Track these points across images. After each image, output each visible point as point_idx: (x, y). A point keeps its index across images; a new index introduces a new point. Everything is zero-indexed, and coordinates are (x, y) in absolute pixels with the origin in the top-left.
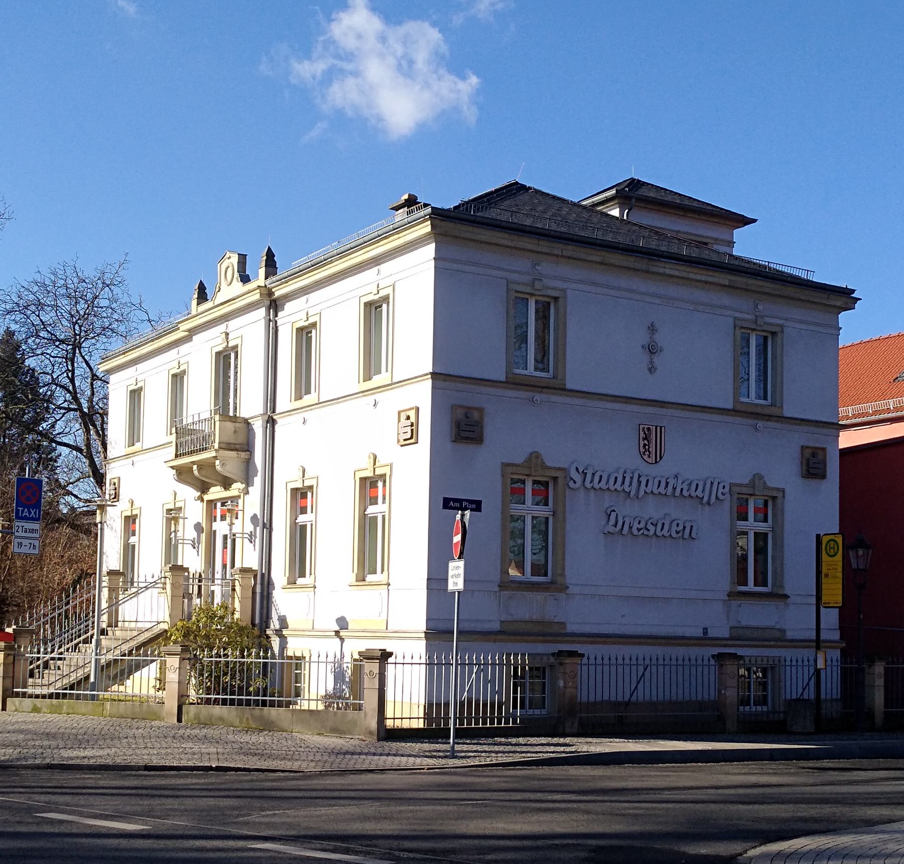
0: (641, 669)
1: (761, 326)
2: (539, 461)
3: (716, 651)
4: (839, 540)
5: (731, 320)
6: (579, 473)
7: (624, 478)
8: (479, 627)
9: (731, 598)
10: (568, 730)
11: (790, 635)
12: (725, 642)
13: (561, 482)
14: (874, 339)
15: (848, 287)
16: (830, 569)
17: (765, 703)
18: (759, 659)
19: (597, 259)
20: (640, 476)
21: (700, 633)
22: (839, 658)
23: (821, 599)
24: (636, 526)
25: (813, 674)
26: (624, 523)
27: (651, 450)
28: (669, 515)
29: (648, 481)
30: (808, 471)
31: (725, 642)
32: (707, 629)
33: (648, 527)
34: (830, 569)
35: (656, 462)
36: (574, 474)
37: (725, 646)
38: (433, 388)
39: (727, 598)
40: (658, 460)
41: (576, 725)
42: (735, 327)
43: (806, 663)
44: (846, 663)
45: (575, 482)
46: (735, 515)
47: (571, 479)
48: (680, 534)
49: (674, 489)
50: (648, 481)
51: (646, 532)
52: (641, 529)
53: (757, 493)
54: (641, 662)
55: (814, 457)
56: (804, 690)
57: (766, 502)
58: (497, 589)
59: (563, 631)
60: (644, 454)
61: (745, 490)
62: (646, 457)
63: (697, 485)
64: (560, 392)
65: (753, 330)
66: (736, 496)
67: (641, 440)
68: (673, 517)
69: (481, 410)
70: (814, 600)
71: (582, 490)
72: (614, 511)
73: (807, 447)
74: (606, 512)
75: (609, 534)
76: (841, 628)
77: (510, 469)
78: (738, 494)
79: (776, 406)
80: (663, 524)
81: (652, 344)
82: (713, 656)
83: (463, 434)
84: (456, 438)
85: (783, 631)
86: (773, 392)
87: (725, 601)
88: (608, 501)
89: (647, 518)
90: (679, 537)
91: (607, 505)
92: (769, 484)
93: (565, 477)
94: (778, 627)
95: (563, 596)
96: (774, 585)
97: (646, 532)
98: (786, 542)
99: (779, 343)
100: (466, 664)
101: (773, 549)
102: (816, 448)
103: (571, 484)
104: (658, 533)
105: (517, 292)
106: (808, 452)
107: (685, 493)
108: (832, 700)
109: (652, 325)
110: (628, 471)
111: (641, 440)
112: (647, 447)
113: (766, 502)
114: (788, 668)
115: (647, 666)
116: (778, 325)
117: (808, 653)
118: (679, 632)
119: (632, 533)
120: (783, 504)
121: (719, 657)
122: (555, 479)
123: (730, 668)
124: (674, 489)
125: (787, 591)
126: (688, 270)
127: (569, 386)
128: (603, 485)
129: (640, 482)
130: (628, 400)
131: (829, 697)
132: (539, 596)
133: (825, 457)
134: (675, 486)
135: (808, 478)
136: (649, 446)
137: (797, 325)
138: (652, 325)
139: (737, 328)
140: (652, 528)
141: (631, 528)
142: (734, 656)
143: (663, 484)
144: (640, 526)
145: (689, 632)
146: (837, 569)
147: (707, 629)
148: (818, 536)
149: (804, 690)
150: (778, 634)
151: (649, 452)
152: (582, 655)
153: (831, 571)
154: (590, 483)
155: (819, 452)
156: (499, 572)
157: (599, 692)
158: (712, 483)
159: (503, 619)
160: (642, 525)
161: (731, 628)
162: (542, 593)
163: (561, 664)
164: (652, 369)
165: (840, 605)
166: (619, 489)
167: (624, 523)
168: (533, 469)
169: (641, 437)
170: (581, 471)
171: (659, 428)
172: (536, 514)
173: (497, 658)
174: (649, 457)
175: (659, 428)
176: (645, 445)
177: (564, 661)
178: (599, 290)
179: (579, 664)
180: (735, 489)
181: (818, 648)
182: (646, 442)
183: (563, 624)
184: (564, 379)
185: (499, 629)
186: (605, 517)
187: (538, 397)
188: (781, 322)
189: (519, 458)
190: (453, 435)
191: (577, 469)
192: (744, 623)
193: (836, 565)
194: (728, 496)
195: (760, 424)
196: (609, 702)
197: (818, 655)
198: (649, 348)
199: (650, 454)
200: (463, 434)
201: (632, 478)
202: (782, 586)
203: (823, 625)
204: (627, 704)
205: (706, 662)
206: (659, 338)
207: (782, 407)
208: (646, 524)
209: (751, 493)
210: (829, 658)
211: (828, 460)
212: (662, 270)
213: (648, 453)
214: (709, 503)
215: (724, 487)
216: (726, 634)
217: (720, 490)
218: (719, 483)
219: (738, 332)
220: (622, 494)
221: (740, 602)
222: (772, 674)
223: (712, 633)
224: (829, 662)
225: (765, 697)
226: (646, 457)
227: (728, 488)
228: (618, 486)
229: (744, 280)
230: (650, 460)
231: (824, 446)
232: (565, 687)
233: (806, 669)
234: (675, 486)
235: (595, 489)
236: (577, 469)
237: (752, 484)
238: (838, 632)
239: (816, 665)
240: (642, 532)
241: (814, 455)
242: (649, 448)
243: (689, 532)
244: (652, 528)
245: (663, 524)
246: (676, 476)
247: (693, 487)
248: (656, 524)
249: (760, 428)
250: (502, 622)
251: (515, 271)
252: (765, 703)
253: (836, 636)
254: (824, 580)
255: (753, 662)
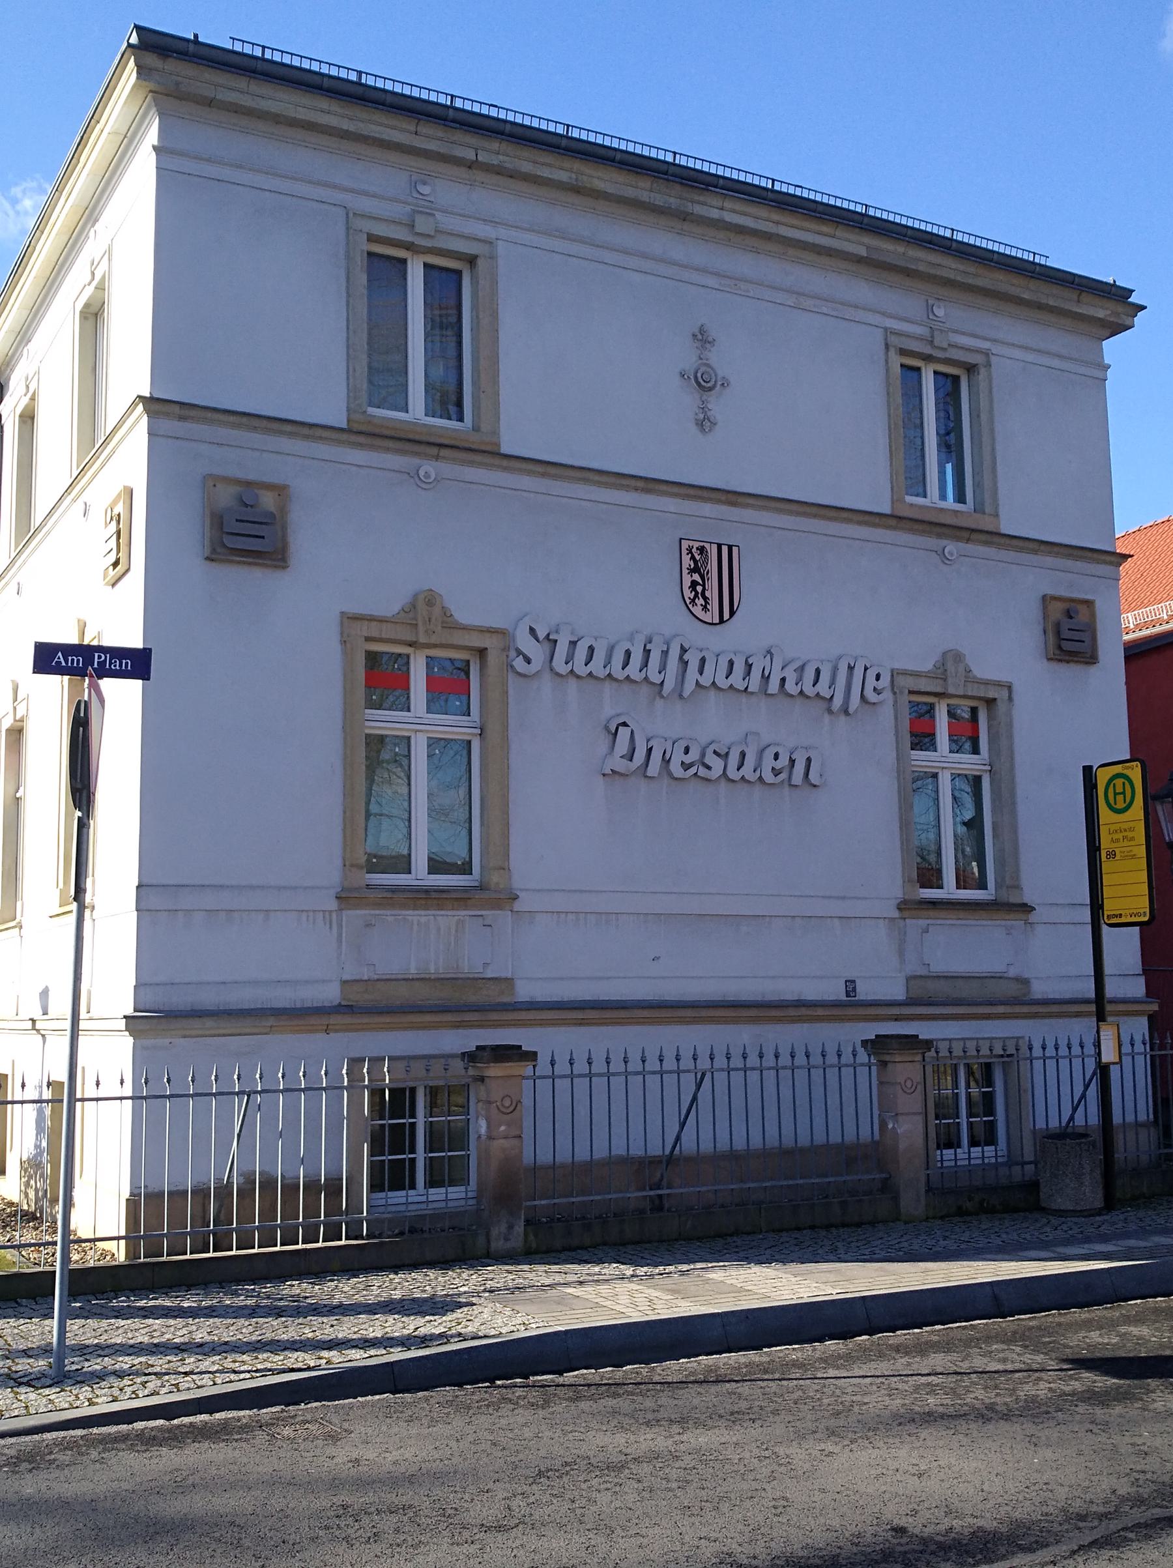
0: (688, 1081)
1: (944, 349)
2: (437, 611)
3: (872, 1030)
4: (1135, 772)
5: (879, 335)
6: (538, 641)
7: (647, 652)
8: (283, 998)
9: (906, 914)
10: (497, 1245)
11: (1039, 990)
12: (895, 1011)
13: (493, 658)
14: (1159, 521)
15: (1117, 283)
16: (1118, 840)
17: (991, 1140)
18: (971, 1046)
19: (563, 176)
20: (684, 650)
21: (835, 991)
22: (1147, 1038)
23: (1102, 907)
24: (678, 758)
25: (1094, 1073)
26: (650, 750)
27: (708, 594)
28: (757, 734)
29: (703, 661)
30: (1060, 648)
31: (895, 1011)
32: (853, 982)
33: (707, 761)
34: (1118, 840)
35: (722, 621)
36: (526, 643)
37: (897, 1019)
38: (151, 433)
39: (896, 914)
40: (726, 616)
41: (520, 1228)
42: (887, 346)
43: (1076, 1050)
44: (1162, 1047)
45: (528, 661)
46: (907, 740)
47: (519, 653)
48: (783, 776)
49: (766, 678)
50: (703, 661)
51: (702, 772)
52: (691, 765)
53: (951, 690)
54: (688, 1063)
55: (1071, 617)
56: (1075, 1109)
57: (974, 711)
58: (333, 905)
59: (506, 999)
60: (693, 601)
61: (924, 685)
62: (697, 610)
63: (818, 672)
64: (487, 459)
65: (928, 358)
66: (905, 698)
67: (685, 571)
68: (766, 738)
69: (281, 490)
70: (1086, 915)
71: (547, 676)
72: (625, 724)
73: (1055, 598)
74: (607, 728)
75: (617, 777)
76: (1148, 971)
77: (365, 629)
78: (910, 692)
79: (984, 513)
80: (743, 755)
81: (703, 369)
82: (865, 1043)
83: (230, 542)
84: (214, 551)
85: (1025, 982)
86: (977, 485)
87: (892, 919)
88: (610, 704)
89: (704, 741)
90: (782, 782)
91: (608, 710)
92: (978, 673)
93: (506, 649)
94: (1012, 973)
95: (503, 918)
96: (998, 886)
97: (702, 772)
98: (1020, 793)
99: (983, 385)
100: (278, 1091)
101: (994, 811)
102: (1072, 600)
103: (519, 663)
104: (732, 773)
105: (372, 238)
106: (1057, 610)
107: (790, 687)
108: (1137, 1124)
109: (702, 330)
110: (655, 639)
111: (685, 571)
112: (699, 588)
113: (974, 711)
114: (1038, 1064)
115: (703, 1075)
116: (978, 351)
117: (1082, 1028)
118: (790, 990)
119: (670, 774)
120: (1009, 714)
121: (878, 1045)
122: (482, 652)
123: (906, 1070)
124: (766, 678)
125: (1027, 899)
126: (775, 216)
127: (505, 449)
128: (597, 666)
129: (685, 664)
130: (650, 485)
131: (1130, 1118)
132: (446, 920)
133: (1093, 615)
134: (766, 673)
135: (1060, 661)
136: (704, 586)
137: (1018, 353)
138: (702, 330)
139: (892, 353)
140: (717, 764)
141: (666, 761)
142: (911, 1042)
143: (739, 668)
144: (688, 759)
145: (812, 991)
146: (1132, 839)
147: (853, 982)
148: (1087, 770)
149: (1075, 1109)
150: (1012, 990)
151: (705, 598)
152: (532, 1056)
153: (1121, 844)
154: (567, 663)
155: (1083, 609)
156: (338, 862)
157: (619, 1129)
158: (851, 668)
159: (346, 977)
160: (693, 756)
161: (909, 979)
162: (450, 913)
163: (482, 1079)
164: (705, 423)
165: (1146, 919)
166: (637, 676)
167: (650, 750)
168: (421, 628)
169: (685, 565)
170: (542, 635)
171: (725, 550)
172: (440, 733)
173: (344, 1071)
174: (705, 608)
175: (725, 550)
176: (694, 584)
177: (487, 1073)
178: (575, 248)
179: (527, 1078)
180: (902, 681)
181: (1101, 1017)
182: (696, 577)
183: (509, 982)
184: (495, 432)
185: (336, 1003)
186: (604, 742)
187: (429, 468)
188: (986, 345)
189: (389, 604)
190: (207, 543)
191: (532, 631)
192: (938, 967)
193: (1131, 829)
194: (887, 695)
195: (951, 547)
196: (626, 1161)
197: (1102, 1033)
198: (696, 378)
199: (706, 603)
200: (230, 542)
201: (665, 653)
202: (1017, 887)
203: (1108, 969)
204: (670, 1160)
205: (847, 1058)
206: (721, 361)
207: (996, 515)
208: (703, 755)
209: (939, 690)
210: (1126, 1040)
211: (1099, 627)
212: (715, 214)
213: (701, 600)
214: (846, 712)
215: (878, 677)
216: (899, 994)
217: (871, 682)
218: (866, 669)
219: (896, 361)
220: (645, 689)
221: (929, 921)
222: (1005, 1074)
223: (864, 992)
224: (1126, 1048)
225: (991, 1127)
226: (697, 610)
227: (889, 678)
228: (633, 670)
229: (901, 249)
230: (707, 617)
231: (1089, 597)
232: (490, 1138)
233: (1077, 1063)
234: (766, 673)
235: (578, 677)
236: (532, 631)
237: (941, 672)
238: (1142, 980)
239: (1099, 1054)
240: (693, 770)
241: (1069, 615)
242: (704, 590)
243: (802, 771)
244: (717, 764)
245: (743, 755)
246: (769, 652)
247: (809, 675)
248: (727, 754)
249: (952, 555)
250: (345, 983)
251: (365, 193)
252: (991, 1140)
253: (1137, 988)
254: (1106, 866)
255: (958, 1052)
